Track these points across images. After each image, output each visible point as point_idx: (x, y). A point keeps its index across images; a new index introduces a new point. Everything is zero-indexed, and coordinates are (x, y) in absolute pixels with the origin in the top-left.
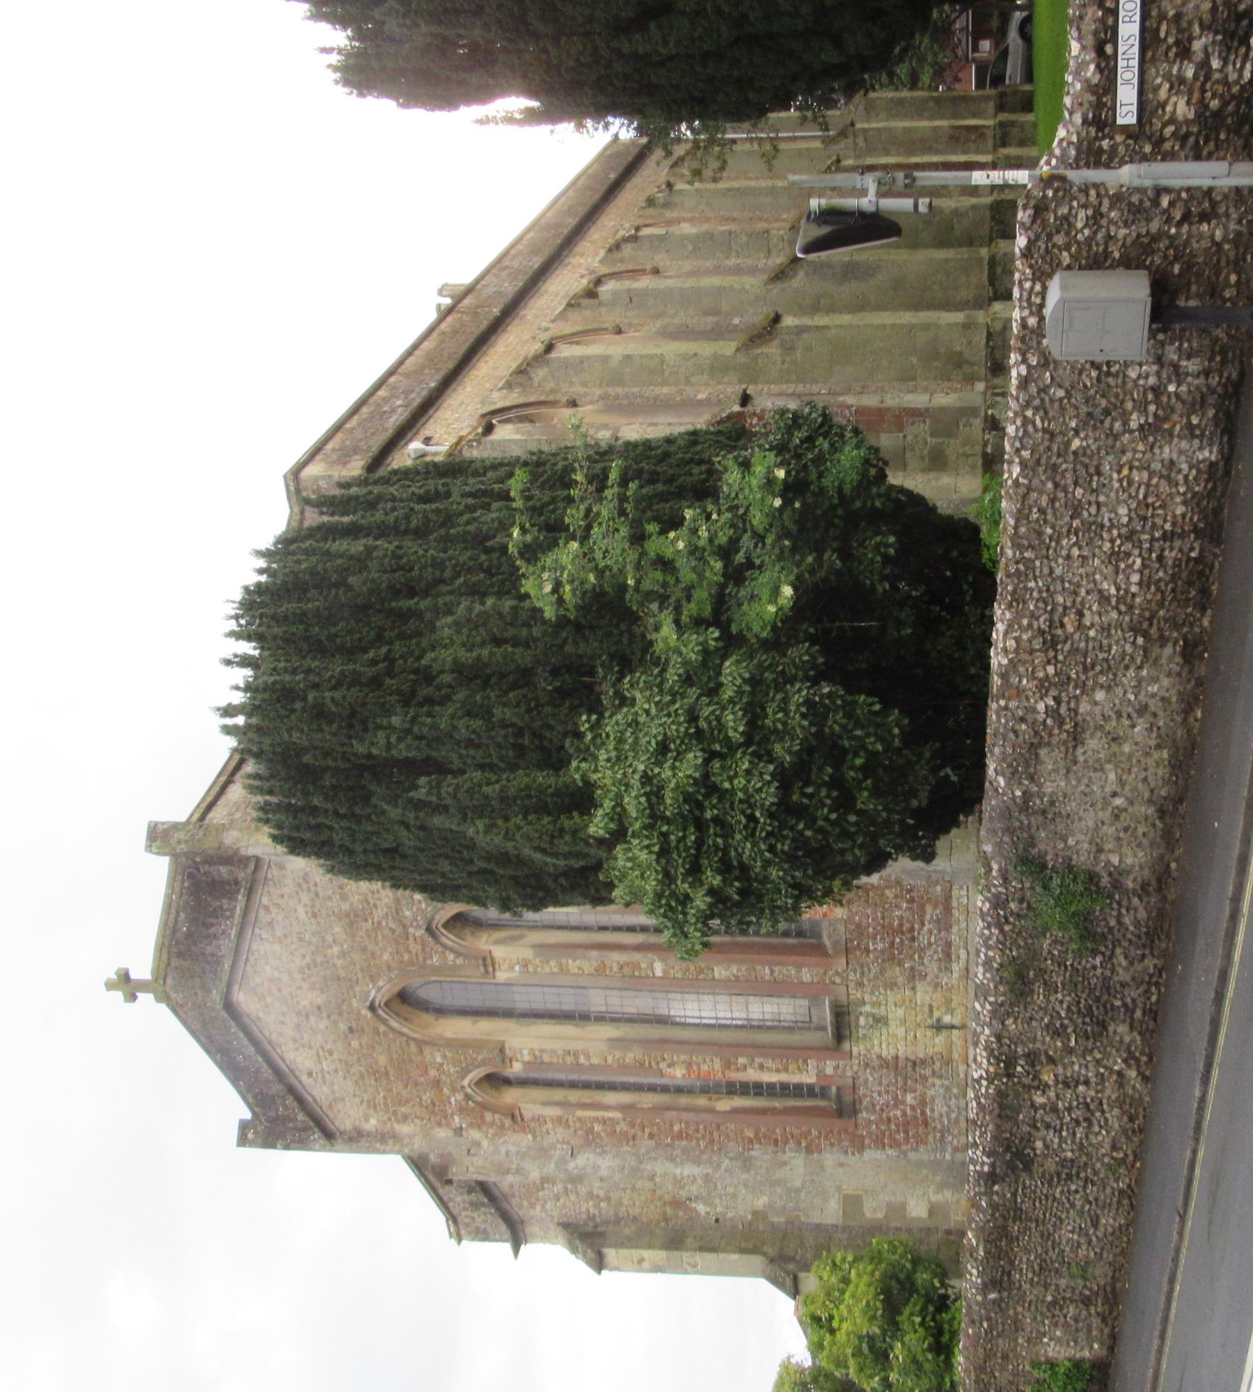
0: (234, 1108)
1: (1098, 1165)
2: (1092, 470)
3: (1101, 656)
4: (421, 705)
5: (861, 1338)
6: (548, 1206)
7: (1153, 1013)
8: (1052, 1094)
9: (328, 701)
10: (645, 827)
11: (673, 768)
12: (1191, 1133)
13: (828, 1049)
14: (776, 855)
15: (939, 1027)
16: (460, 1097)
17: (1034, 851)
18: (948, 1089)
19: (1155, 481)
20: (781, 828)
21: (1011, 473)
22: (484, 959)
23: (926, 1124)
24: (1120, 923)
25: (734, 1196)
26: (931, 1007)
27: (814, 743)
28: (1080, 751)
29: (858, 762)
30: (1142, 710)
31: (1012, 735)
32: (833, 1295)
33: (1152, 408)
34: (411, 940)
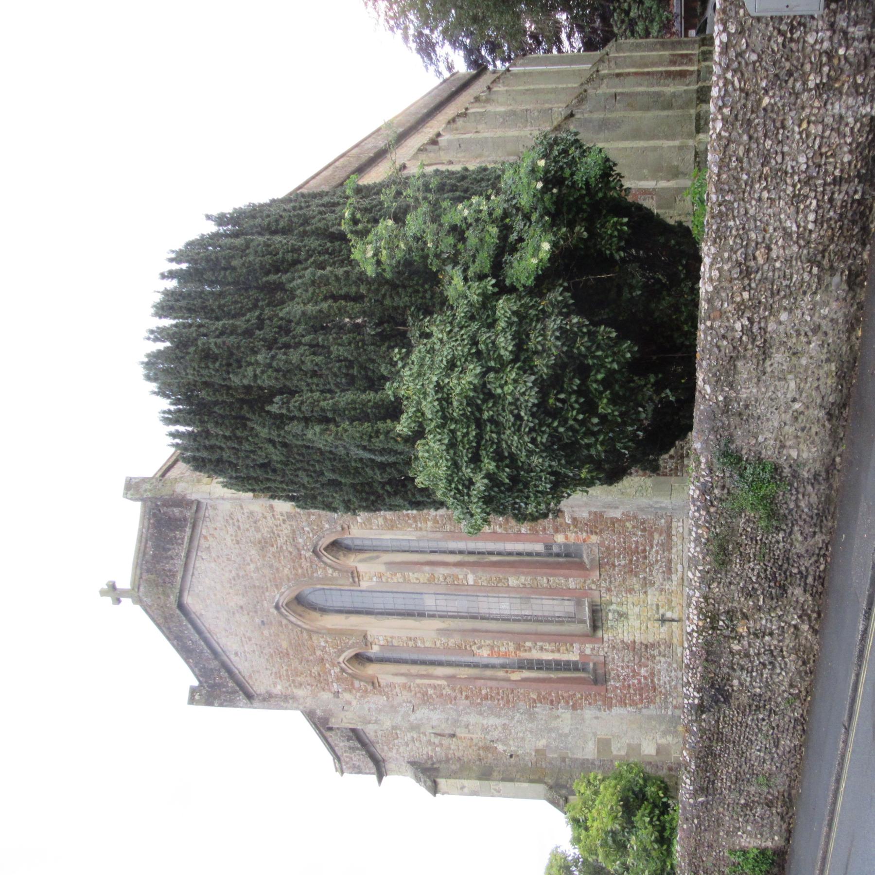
0: (186, 678)
1: (780, 699)
2: (778, 124)
3: (785, 283)
4: (280, 348)
5: (607, 833)
6: (401, 750)
7: (821, 579)
8: (745, 643)
9: (212, 346)
10: (438, 427)
11: (459, 379)
12: (855, 660)
13: (587, 636)
14: (537, 446)
15: (663, 620)
16: (337, 670)
17: (733, 447)
18: (670, 664)
19: (827, 133)
20: (541, 425)
21: (714, 128)
22: (352, 573)
23: (655, 689)
24: (798, 506)
25: (523, 739)
26: (657, 605)
27: (566, 360)
28: (768, 363)
29: (600, 377)
30: (816, 329)
31: (716, 350)
32: (588, 805)
33: (826, 69)
34: (303, 560)
